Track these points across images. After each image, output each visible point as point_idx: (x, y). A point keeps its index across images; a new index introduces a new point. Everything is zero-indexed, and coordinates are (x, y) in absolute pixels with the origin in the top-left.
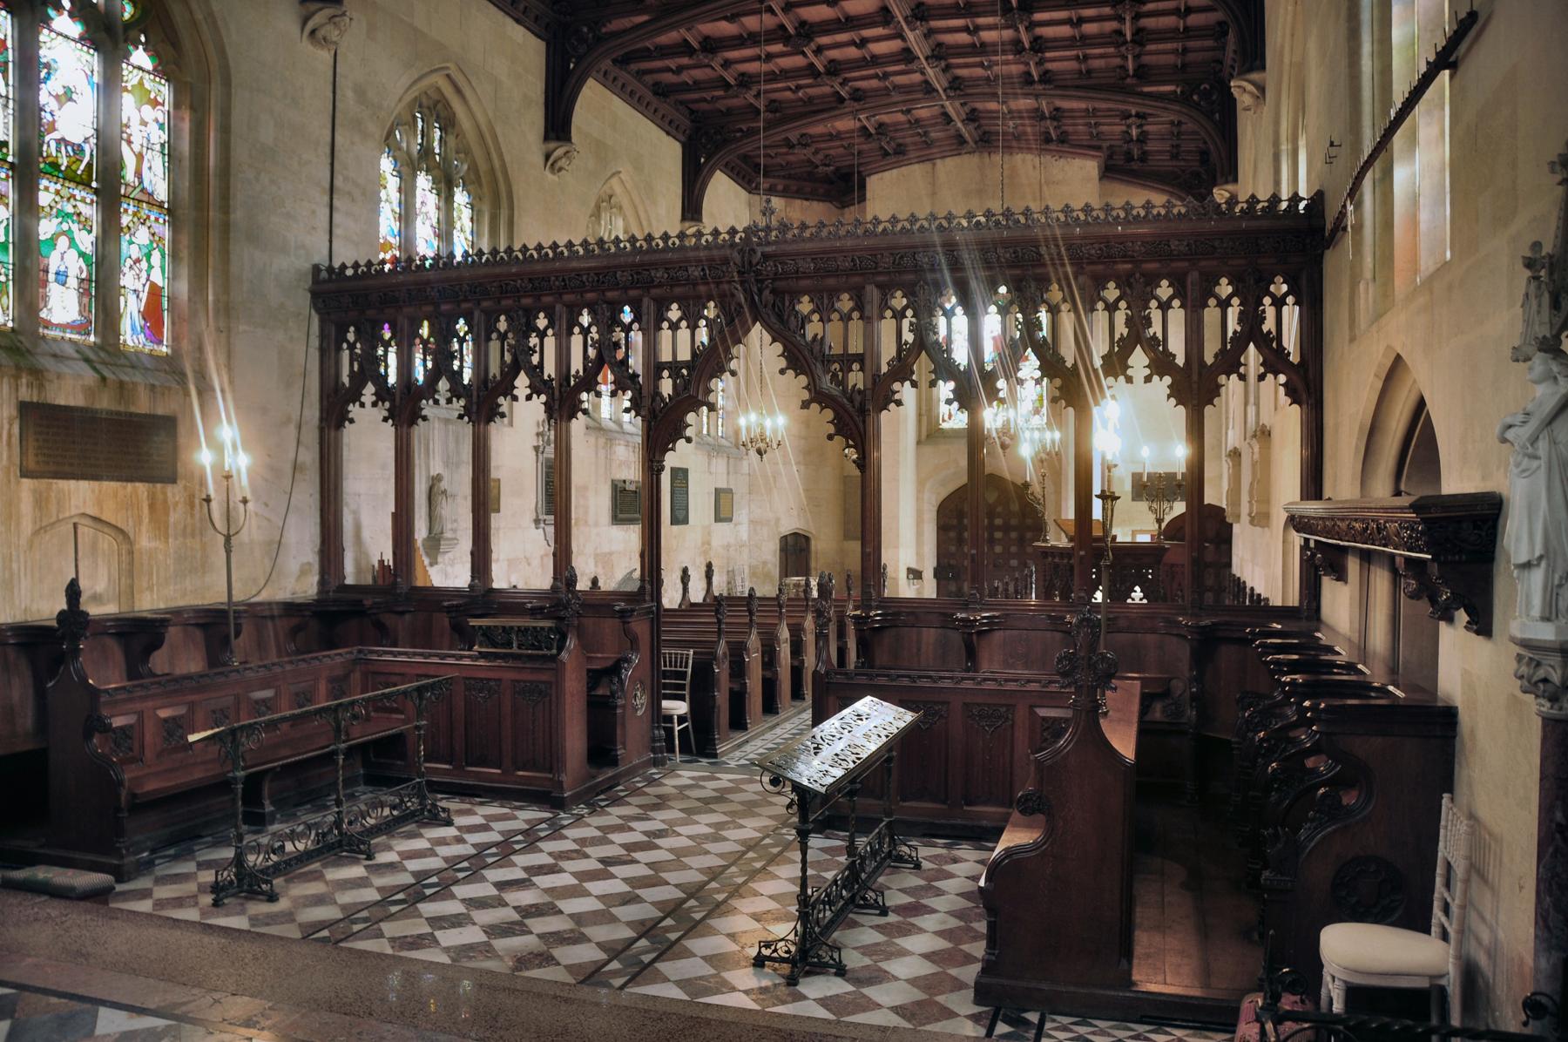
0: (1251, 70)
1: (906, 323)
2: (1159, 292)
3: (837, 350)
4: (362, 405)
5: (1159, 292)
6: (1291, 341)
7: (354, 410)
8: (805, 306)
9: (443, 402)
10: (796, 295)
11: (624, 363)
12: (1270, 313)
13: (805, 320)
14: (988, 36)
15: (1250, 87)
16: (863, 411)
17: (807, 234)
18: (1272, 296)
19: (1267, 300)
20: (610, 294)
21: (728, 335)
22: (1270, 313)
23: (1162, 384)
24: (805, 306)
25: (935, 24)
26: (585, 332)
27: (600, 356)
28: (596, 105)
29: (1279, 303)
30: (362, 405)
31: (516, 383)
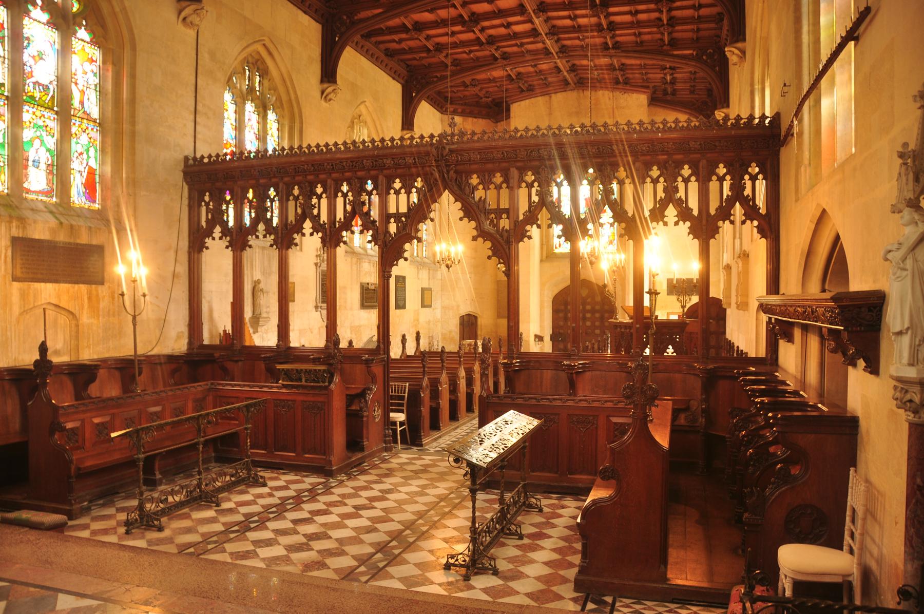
0: (737, 41)
1: (534, 191)
2: (683, 172)
3: (493, 206)
4: (214, 239)
5: (651, 173)
7: (209, 241)
8: (474, 180)
9: (261, 237)
10: (469, 174)
11: (368, 214)
12: (749, 184)
13: (475, 188)
15: (736, 51)
16: (508, 242)
19: (747, 177)
21: (429, 197)
22: (749, 184)
23: (685, 227)
24: (474, 180)
26: (345, 196)
28: (351, 62)
29: (754, 178)
30: (214, 239)
31: (304, 226)
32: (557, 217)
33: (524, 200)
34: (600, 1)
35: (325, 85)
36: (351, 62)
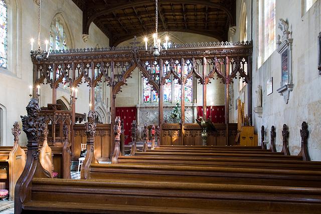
0: (233, 26)
3: (154, 72)
4: (236, 78)
6: (246, 70)
8: (147, 64)
9: (45, 84)
10: (145, 61)
12: (242, 65)
13: (147, 66)
14: (177, 17)
16: (159, 85)
17: (93, 50)
18: (242, 62)
19: (241, 63)
20: (65, 62)
21: (130, 70)
22: (242, 65)
24: (147, 64)
25: (166, 13)
27: (44, 76)
28: (93, 27)
29: (243, 63)
30: (236, 78)
32: (243, 75)
33: (166, 69)
34: (316, 5)
35: (85, 35)
36: (93, 27)
